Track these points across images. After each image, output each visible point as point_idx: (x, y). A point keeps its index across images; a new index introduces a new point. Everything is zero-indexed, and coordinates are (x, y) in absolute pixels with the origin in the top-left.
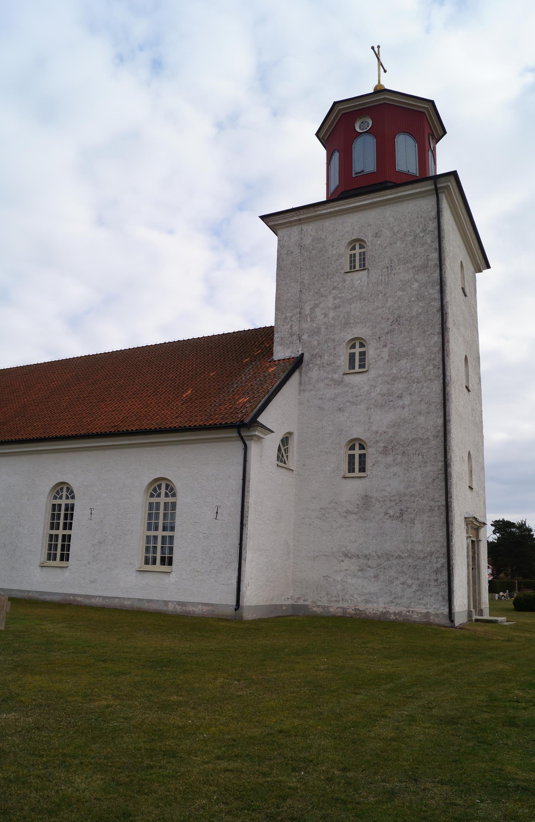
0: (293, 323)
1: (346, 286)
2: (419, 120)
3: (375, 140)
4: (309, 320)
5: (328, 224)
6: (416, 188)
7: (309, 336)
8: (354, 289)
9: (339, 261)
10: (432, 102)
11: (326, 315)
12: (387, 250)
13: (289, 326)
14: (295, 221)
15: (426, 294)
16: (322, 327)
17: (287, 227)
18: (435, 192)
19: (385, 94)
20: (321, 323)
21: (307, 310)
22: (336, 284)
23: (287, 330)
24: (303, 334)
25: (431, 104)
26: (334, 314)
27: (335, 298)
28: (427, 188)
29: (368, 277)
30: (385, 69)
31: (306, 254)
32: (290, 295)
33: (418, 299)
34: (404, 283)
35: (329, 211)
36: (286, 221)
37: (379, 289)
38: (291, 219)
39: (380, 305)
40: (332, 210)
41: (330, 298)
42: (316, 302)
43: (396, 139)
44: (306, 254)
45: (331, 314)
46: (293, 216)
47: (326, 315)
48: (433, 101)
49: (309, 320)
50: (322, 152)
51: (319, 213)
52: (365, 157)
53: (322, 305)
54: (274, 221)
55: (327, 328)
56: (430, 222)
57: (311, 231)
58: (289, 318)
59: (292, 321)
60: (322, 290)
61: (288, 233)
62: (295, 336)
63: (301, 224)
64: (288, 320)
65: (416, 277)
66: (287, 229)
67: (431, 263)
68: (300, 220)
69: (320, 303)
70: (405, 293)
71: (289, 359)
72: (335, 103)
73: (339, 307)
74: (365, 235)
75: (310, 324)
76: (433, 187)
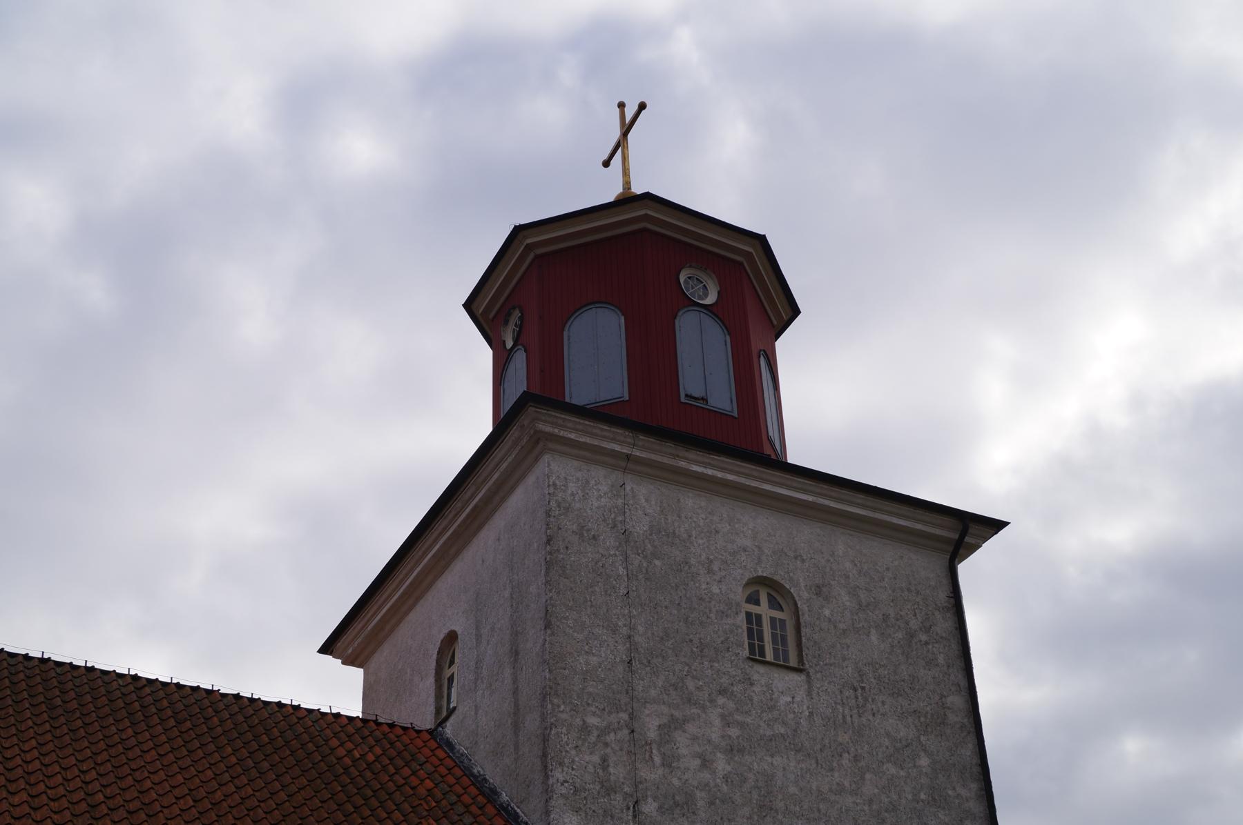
0: (608, 750)
1: (755, 699)
4: (657, 760)
5: (691, 502)
6: (919, 521)
7: (660, 809)
8: (776, 713)
9: (730, 621)
11: (706, 763)
12: (848, 641)
13: (596, 759)
14: (614, 454)
15: (950, 792)
16: (698, 794)
17: (577, 457)
18: (951, 549)
19: (526, 237)
20: (695, 783)
21: (651, 726)
22: (725, 680)
23: (591, 769)
24: (645, 797)
26: (729, 768)
27: (727, 722)
28: (938, 532)
29: (809, 693)
31: (636, 560)
32: (594, 660)
33: (934, 799)
34: (898, 745)
35: (710, 472)
37: (840, 739)
38: (605, 445)
39: (846, 784)
40: (720, 475)
41: (714, 715)
42: (677, 714)
43: (565, 334)
44: (636, 560)
45: (722, 765)
46: (614, 440)
47: (706, 763)
49: (657, 760)
51: (682, 464)
52: (597, 351)
53: (691, 728)
55: (711, 803)
56: (938, 615)
57: (647, 500)
58: (595, 733)
59: (606, 745)
60: (691, 684)
61: (579, 474)
62: (619, 797)
63: (625, 470)
64: (593, 739)
65: (922, 738)
66: (576, 463)
67: (952, 718)
68: (628, 457)
69: (685, 720)
70: (902, 773)
71: (405, 729)
73: (741, 751)
74: (791, 579)
75: (660, 772)
76: (957, 536)
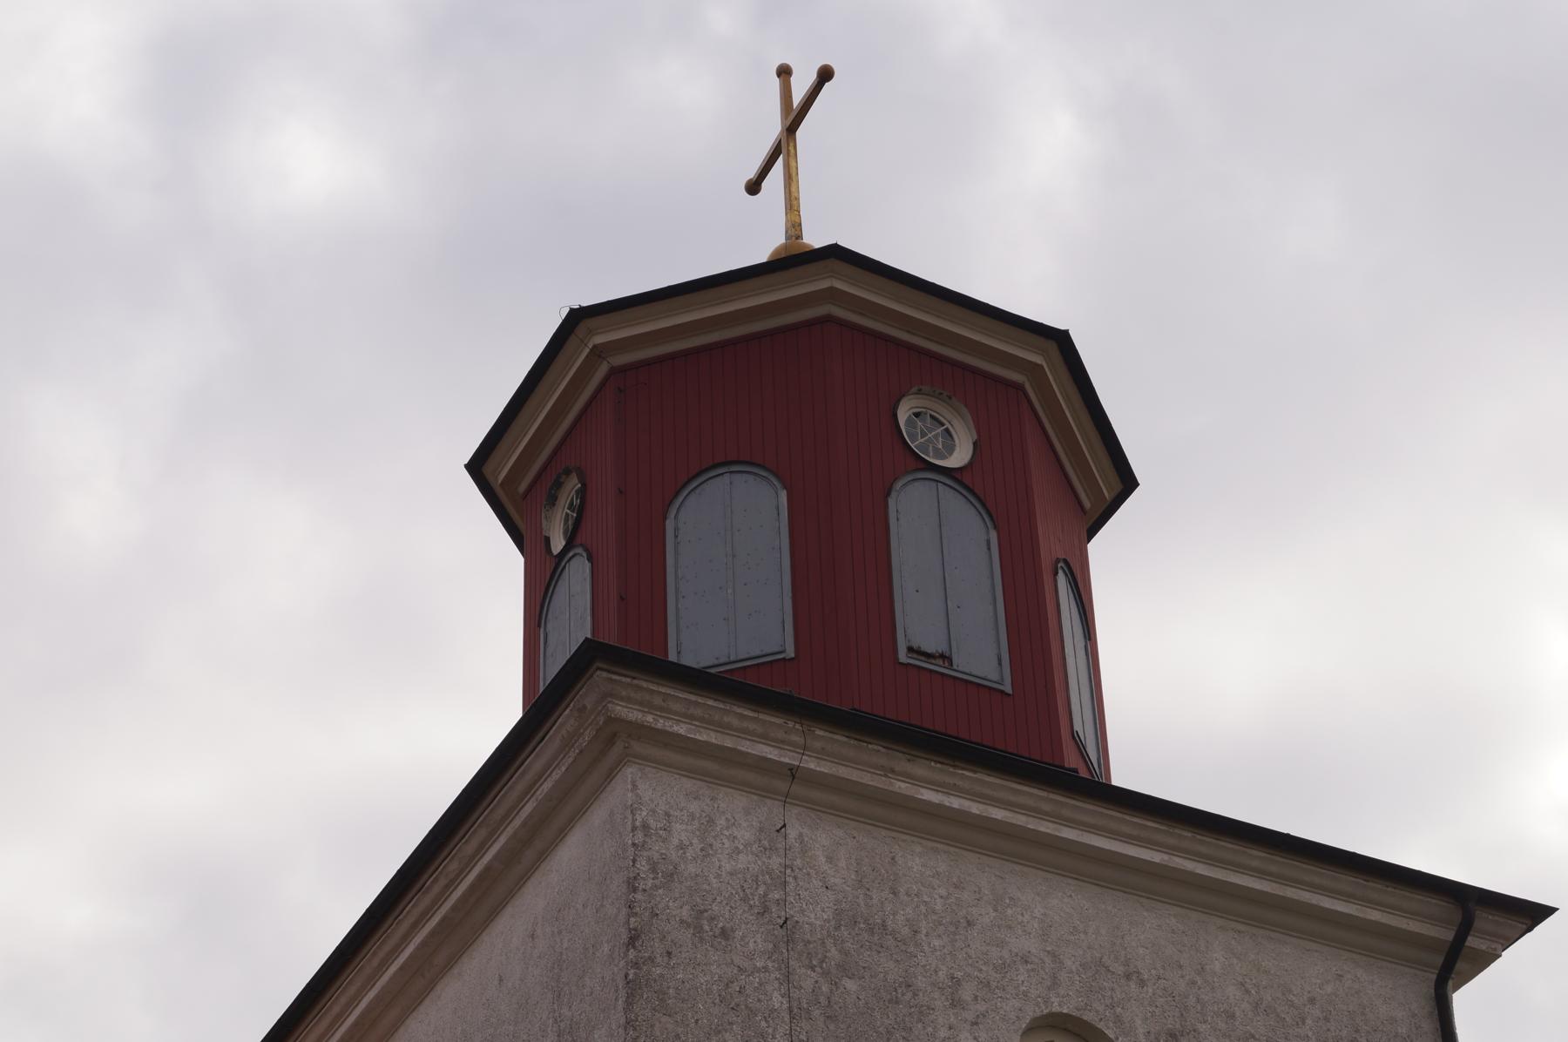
2: (1030, 431)
3: (783, 496)
10: (1062, 340)
17: (691, 773)
25: (1052, 347)
30: (776, 82)
35: (955, 803)
36: (712, 737)
38: (746, 746)
40: (975, 808)
44: (807, 979)
46: (765, 738)
48: (1066, 334)
50: (501, 566)
51: (901, 787)
52: (731, 564)
54: (649, 707)
63: (787, 799)
66: (688, 784)
68: (793, 773)
72: (576, 318)
76: (1448, 935)
